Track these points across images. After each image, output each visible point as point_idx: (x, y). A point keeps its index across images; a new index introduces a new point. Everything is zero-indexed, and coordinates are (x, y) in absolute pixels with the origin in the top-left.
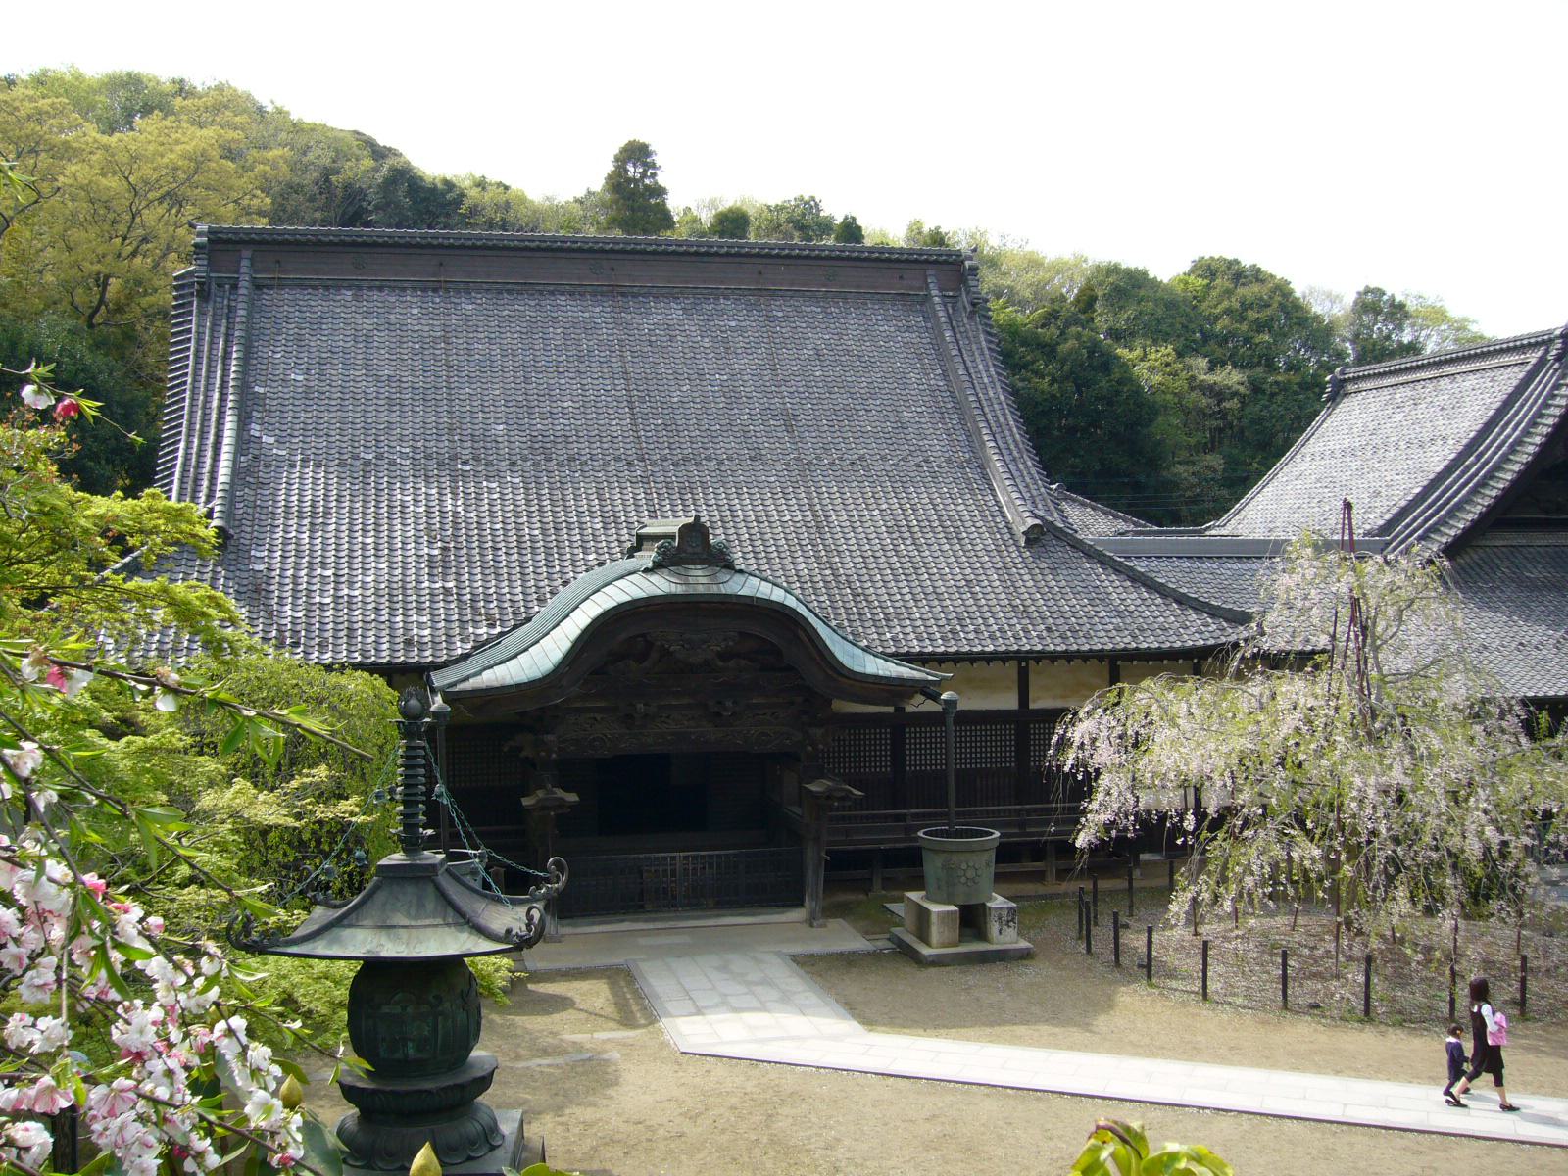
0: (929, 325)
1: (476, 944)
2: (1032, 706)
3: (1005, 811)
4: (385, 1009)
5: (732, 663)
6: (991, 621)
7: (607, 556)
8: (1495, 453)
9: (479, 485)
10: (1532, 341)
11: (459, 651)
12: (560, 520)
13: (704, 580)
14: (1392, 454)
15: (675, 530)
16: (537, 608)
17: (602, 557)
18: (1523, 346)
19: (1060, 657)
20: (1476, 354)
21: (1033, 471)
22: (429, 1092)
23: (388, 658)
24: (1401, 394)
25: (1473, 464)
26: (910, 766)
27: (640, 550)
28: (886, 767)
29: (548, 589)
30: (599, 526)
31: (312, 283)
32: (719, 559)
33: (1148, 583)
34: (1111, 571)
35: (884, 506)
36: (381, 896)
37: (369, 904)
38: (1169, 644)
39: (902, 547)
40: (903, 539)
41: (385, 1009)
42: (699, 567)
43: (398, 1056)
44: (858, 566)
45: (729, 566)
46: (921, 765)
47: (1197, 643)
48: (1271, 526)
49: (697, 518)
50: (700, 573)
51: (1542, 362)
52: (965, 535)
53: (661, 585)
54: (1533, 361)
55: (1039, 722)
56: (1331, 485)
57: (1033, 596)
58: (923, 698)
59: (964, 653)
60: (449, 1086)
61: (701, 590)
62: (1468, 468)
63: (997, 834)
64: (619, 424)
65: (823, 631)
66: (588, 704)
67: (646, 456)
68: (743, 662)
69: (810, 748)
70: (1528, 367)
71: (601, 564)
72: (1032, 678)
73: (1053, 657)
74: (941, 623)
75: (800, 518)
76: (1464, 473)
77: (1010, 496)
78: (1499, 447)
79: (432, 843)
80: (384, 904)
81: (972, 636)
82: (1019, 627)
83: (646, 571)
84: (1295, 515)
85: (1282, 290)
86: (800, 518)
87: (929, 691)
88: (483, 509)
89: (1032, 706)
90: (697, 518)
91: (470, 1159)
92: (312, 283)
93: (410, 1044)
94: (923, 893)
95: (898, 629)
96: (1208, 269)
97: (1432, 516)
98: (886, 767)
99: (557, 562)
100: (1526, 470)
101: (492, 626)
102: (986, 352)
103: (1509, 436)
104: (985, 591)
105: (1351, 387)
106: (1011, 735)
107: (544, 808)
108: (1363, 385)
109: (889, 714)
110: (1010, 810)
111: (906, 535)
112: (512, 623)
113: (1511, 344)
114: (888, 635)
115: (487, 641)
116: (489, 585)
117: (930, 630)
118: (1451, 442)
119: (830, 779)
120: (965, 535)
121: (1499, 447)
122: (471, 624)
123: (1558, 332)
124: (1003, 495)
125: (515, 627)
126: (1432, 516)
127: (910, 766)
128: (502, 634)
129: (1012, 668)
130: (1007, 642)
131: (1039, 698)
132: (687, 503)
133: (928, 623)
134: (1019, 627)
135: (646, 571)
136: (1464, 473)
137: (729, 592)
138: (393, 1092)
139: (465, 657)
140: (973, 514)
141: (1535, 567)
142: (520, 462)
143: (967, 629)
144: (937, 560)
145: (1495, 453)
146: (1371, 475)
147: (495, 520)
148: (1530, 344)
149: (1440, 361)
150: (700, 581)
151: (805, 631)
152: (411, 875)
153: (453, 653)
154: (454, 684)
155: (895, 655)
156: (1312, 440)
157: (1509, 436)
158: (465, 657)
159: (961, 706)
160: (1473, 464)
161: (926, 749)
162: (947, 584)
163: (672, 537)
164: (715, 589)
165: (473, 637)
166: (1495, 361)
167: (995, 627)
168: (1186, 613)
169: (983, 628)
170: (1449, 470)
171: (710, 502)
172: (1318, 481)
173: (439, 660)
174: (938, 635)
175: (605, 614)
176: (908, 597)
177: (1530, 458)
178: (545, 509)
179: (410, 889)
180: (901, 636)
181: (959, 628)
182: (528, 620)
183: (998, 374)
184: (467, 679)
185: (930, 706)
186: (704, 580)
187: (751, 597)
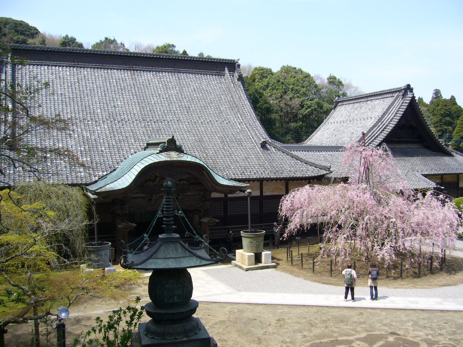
0: (226, 82)
1: (201, 262)
2: (264, 194)
3: (256, 226)
4: (167, 286)
5: (181, 182)
6: (254, 169)
7: (137, 150)
8: (386, 122)
9: (94, 128)
10: (395, 90)
11: (94, 180)
12: (121, 139)
13: (176, 156)
14: (356, 122)
15: (166, 141)
16: (117, 166)
17: (135, 151)
18: (392, 92)
19: (251, 180)
20: (378, 94)
21: (260, 126)
22: (183, 313)
23: (71, 182)
24: (356, 105)
25: (381, 125)
26: (265, 211)
27: (147, 148)
28: (222, 213)
29: (120, 160)
30: (133, 141)
31: (33, 63)
32: (179, 150)
33: (297, 158)
34: (286, 155)
35: (219, 135)
36: (163, 248)
37: (159, 251)
38: (305, 176)
39: (226, 147)
40: (225, 145)
41: (167, 286)
42: (173, 152)
43: (171, 301)
44: (213, 153)
45: (182, 152)
46: (235, 213)
47: (312, 175)
48: (321, 143)
49: (173, 137)
50: (174, 154)
51: (398, 96)
52: (243, 144)
53: (163, 157)
54: (396, 96)
55: (268, 200)
56: (338, 131)
57: (265, 162)
58: (239, 192)
59: (247, 179)
60: (189, 310)
61: (175, 159)
62: (379, 126)
63: (264, 232)
64: (136, 110)
65: (211, 172)
66: (138, 196)
67: (145, 120)
68: (185, 182)
69: (205, 208)
70: (394, 98)
71: (135, 152)
72: (264, 186)
73: (272, 180)
74: (239, 170)
75: (194, 139)
76: (378, 127)
77: (255, 133)
78: (388, 120)
79: (175, 231)
80: (164, 251)
81: (249, 174)
82: (262, 171)
83: (157, 153)
84: (328, 140)
85: (308, 76)
86: (194, 139)
87: (242, 189)
88: (96, 135)
89: (264, 194)
90: (173, 137)
91: (196, 334)
92: (33, 63)
93: (175, 297)
94: (242, 250)
95: (228, 172)
96: (287, 70)
97: (370, 139)
98: (222, 213)
99: (122, 152)
100: (395, 126)
101: (103, 172)
102: (243, 90)
103: (390, 117)
104: (251, 160)
105: (340, 104)
106: (258, 203)
107: (126, 228)
108: (344, 103)
109: (222, 198)
110: (258, 226)
111: (226, 144)
112: (110, 171)
113: (389, 91)
114: (225, 174)
115: (103, 177)
116: (101, 159)
117: (237, 172)
118: (373, 119)
119: (208, 217)
120: (243, 144)
121: (388, 120)
122: (97, 171)
123: (403, 88)
124: (253, 132)
125: (111, 172)
126: (370, 139)
127: (265, 211)
128: (107, 174)
129: (258, 184)
130: (259, 175)
131: (266, 192)
132: (160, 134)
133: (236, 170)
134: (262, 171)
135: (157, 153)
136: (378, 127)
137: (184, 160)
138: (171, 314)
139: (96, 182)
140: (245, 138)
141: (397, 154)
142: (106, 121)
143: (247, 172)
144: (236, 151)
145: (386, 122)
146: (350, 128)
147: (100, 139)
148: (394, 91)
149: (368, 96)
150: (174, 156)
151: (206, 171)
152: (171, 241)
153: (92, 180)
154: (97, 190)
155: (231, 179)
156: (330, 119)
157: (390, 117)
158: (96, 182)
159: (253, 194)
160: (381, 125)
161: (275, 204)
162: (240, 158)
163: (165, 143)
164: (179, 159)
165: (98, 175)
166: (384, 96)
167: (256, 171)
168: (308, 166)
169: (252, 171)
170: (374, 126)
171: (167, 134)
172: (334, 130)
173: (88, 183)
174: (239, 174)
175: (146, 167)
176: (229, 162)
177: (396, 123)
178: (116, 135)
179: (172, 245)
180: (229, 174)
181: (245, 171)
182: (115, 170)
183: (247, 97)
184: (101, 188)
185: (241, 194)
186: (176, 156)
187: (190, 161)
